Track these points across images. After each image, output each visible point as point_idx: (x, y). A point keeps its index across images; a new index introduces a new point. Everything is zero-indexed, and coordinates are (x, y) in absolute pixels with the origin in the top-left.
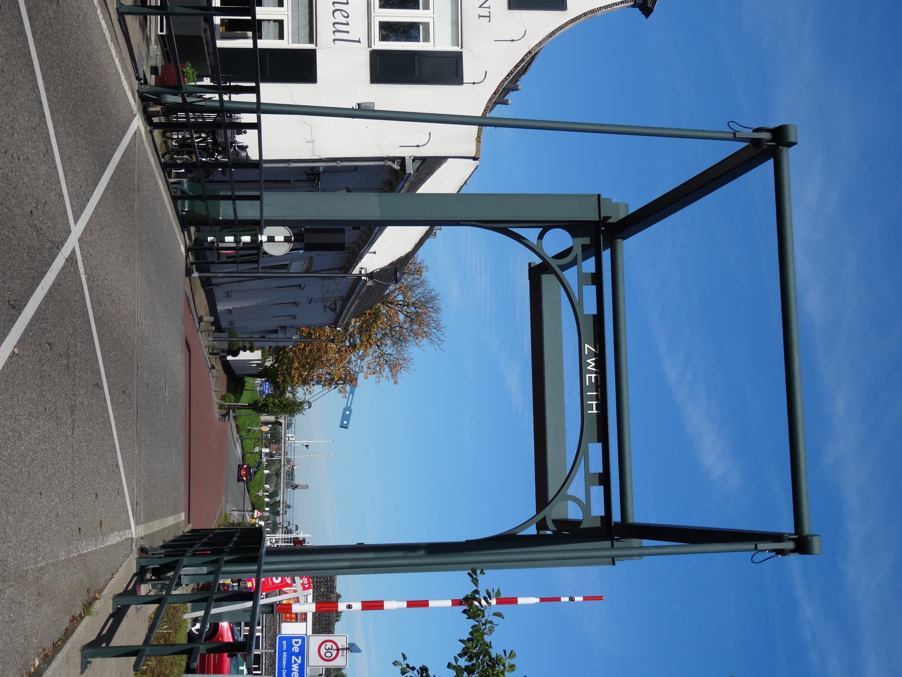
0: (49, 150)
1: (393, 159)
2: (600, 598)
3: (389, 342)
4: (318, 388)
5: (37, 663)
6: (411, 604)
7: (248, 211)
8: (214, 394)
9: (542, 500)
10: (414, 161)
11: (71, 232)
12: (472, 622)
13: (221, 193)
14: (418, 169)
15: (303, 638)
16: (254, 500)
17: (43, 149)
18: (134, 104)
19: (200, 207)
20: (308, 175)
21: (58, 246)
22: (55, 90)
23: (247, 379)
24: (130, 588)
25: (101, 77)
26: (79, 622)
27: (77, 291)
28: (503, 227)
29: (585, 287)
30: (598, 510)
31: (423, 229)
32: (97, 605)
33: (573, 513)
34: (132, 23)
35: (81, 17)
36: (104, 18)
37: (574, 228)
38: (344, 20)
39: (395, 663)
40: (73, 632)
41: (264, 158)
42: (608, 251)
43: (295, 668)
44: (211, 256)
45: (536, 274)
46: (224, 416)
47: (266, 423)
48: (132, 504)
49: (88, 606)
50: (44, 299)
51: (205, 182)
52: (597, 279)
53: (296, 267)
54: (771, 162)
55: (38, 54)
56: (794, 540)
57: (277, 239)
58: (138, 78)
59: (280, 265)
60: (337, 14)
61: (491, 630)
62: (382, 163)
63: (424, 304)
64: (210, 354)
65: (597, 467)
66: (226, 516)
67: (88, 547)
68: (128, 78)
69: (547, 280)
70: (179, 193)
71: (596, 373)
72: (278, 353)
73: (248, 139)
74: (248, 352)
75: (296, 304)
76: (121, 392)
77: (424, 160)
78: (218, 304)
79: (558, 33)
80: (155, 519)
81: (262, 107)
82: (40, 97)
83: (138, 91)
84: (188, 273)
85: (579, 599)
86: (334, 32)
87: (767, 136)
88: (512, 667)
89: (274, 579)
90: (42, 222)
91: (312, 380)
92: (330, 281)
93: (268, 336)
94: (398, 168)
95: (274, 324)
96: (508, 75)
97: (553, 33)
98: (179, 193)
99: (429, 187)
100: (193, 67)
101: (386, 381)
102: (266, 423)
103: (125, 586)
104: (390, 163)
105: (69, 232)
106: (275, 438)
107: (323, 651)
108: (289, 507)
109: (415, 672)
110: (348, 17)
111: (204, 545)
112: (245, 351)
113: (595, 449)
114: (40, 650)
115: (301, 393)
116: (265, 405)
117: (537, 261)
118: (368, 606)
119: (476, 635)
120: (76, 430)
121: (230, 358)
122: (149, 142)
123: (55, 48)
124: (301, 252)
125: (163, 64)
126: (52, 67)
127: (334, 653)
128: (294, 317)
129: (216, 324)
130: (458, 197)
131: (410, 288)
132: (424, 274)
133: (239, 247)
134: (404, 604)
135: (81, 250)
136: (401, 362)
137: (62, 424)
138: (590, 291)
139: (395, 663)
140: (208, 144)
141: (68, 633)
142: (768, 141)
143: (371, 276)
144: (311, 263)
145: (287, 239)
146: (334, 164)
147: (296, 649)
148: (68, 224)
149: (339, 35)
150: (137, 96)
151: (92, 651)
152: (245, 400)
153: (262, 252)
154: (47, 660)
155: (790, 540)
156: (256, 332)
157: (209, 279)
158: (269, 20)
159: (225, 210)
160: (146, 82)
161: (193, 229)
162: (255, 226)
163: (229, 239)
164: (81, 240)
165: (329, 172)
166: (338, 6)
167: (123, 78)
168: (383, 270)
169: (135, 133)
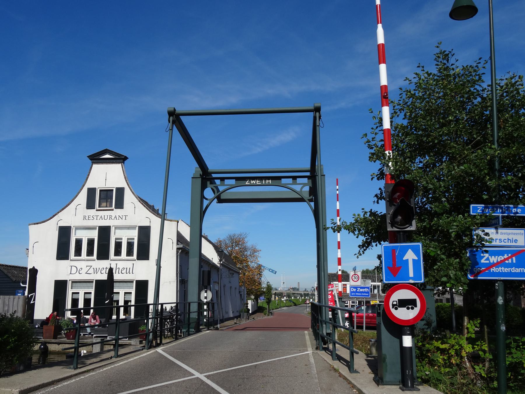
0: (166, 386)
1: (177, 252)
2: (337, 180)
3: (246, 253)
4: (262, 279)
5: (355, 390)
6: (339, 248)
7: (194, 307)
8: (264, 318)
9: (301, 200)
10: (178, 245)
11: (198, 377)
12: (343, 229)
13: (188, 317)
14: (181, 243)
15: (351, 287)
16: (303, 303)
17: (166, 388)
18: (152, 351)
19: (192, 325)
20: (182, 284)
21: (203, 382)
22: (144, 383)
23: (259, 305)
24: (330, 354)
25: (141, 364)
26: (341, 374)
27: (220, 374)
28: (203, 213)
29: (225, 184)
30: (305, 180)
31: (203, 240)
32: (336, 367)
33: (307, 189)
34: (122, 351)
35: (118, 372)
36: (119, 363)
37: (204, 187)
38: (125, 269)
39: (358, 257)
40: (344, 376)
41: (176, 302)
42: (213, 175)
43: (361, 290)
44: (211, 320)
45: (221, 201)
46: (272, 314)
47: (275, 298)
48: (300, 353)
49: (336, 370)
50: (222, 388)
51: (184, 323)
52: (222, 179)
53: (217, 287)
54: (182, 117)
55: (130, 390)
56: (315, 113)
57: (206, 295)
58: (142, 350)
59: (216, 294)
60: (123, 272)
61: (345, 222)
62: (179, 256)
63: (232, 240)
64: (249, 319)
65: (290, 181)
66: (308, 313)
67: (314, 371)
68: (142, 354)
69: (223, 197)
70: (187, 333)
71: (256, 180)
72: (249, 294)
73: (168, 307)
74: (248, 305)
75: (231, 287)
76: (259, 357)
77: (178, 241)
78: (230, 317)
79: (66, 383)
80: (306, 343)
81: (155, 303)
82: (146, 389)
83: (147, 350)
84: (217, 329)
85: (337, 187)
86: (129, 273)
87: (171, 118)
88: (358, 215)
89: (329, 298)
90: (193, 389)
91: (259, 281)
92: (222, 275)
93: (242, 298)
94: (181, 250)
95: (238, 296)
96: (148, 209)
97: (132, 192)
98: (187, 333)
99: (188, 237)
100: (140, 327)
101: (261, 254)
102: (275, 298)
103: (329, 356)
104: (179, 253)
105: (198, 378)
106: (281, 295)
107: (356, 280)
108: (306, 290)
109: (360, 250)
110: (124, 268)
111: (316, 325)
112: (248, 307)
113: (284, 181)
114: (350, 389)
115: (264, 285)
116: (268, 299)
117: (216, 200)
118: (339, 264)
119: (347, 228)
120: (271, 375)
121: (250, 312)
122: (167, 345)
123: (128, 383)
124: (211, 286)
125: (139, 338)
126: (135, 384)
127: (356, 276)
128: (236, 288)
129: (237, 317)
130: (191, 226)
131: (226, 245)
132: (221, 240)
133: (208, 310)
134: (339, 250)
135: (205, 373)
136: (253, 248)
137: (269, 381)
138: (227, 182)
139: (358, 257)
140: (169, 321)
141: (345, 378)
142: (173, 118)
143: (220, 260)
144: (215, 282)
145: (206, 292)
146: (179, 274)
147: (355, 290)
148: (195, 378)
149: (131, 272)
150: (149, 350)
151: (351, 369)
152: (267, 307)
153: (211, 302)
154: (354, 386)
155: (315, 114)
156: (241, 303)
157: (220, 320)
158: (124, 297)
159: (194, 316)
160: (144, 346)
161: (201, 327)
162: (200, 304)
163: (205, 313)
164: (201, 373)
165: (181, 276)
166: (120, 272)
167: (142, 356)
168: (218, 255)
169: (163, 351)
